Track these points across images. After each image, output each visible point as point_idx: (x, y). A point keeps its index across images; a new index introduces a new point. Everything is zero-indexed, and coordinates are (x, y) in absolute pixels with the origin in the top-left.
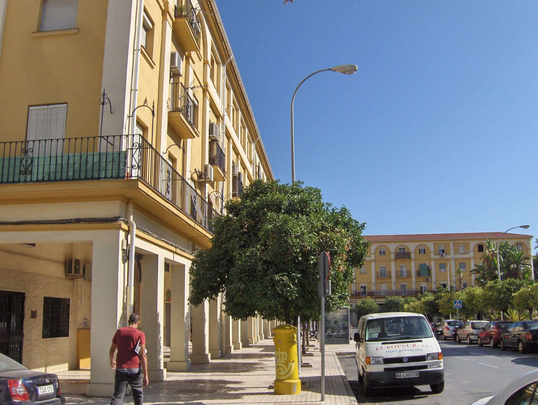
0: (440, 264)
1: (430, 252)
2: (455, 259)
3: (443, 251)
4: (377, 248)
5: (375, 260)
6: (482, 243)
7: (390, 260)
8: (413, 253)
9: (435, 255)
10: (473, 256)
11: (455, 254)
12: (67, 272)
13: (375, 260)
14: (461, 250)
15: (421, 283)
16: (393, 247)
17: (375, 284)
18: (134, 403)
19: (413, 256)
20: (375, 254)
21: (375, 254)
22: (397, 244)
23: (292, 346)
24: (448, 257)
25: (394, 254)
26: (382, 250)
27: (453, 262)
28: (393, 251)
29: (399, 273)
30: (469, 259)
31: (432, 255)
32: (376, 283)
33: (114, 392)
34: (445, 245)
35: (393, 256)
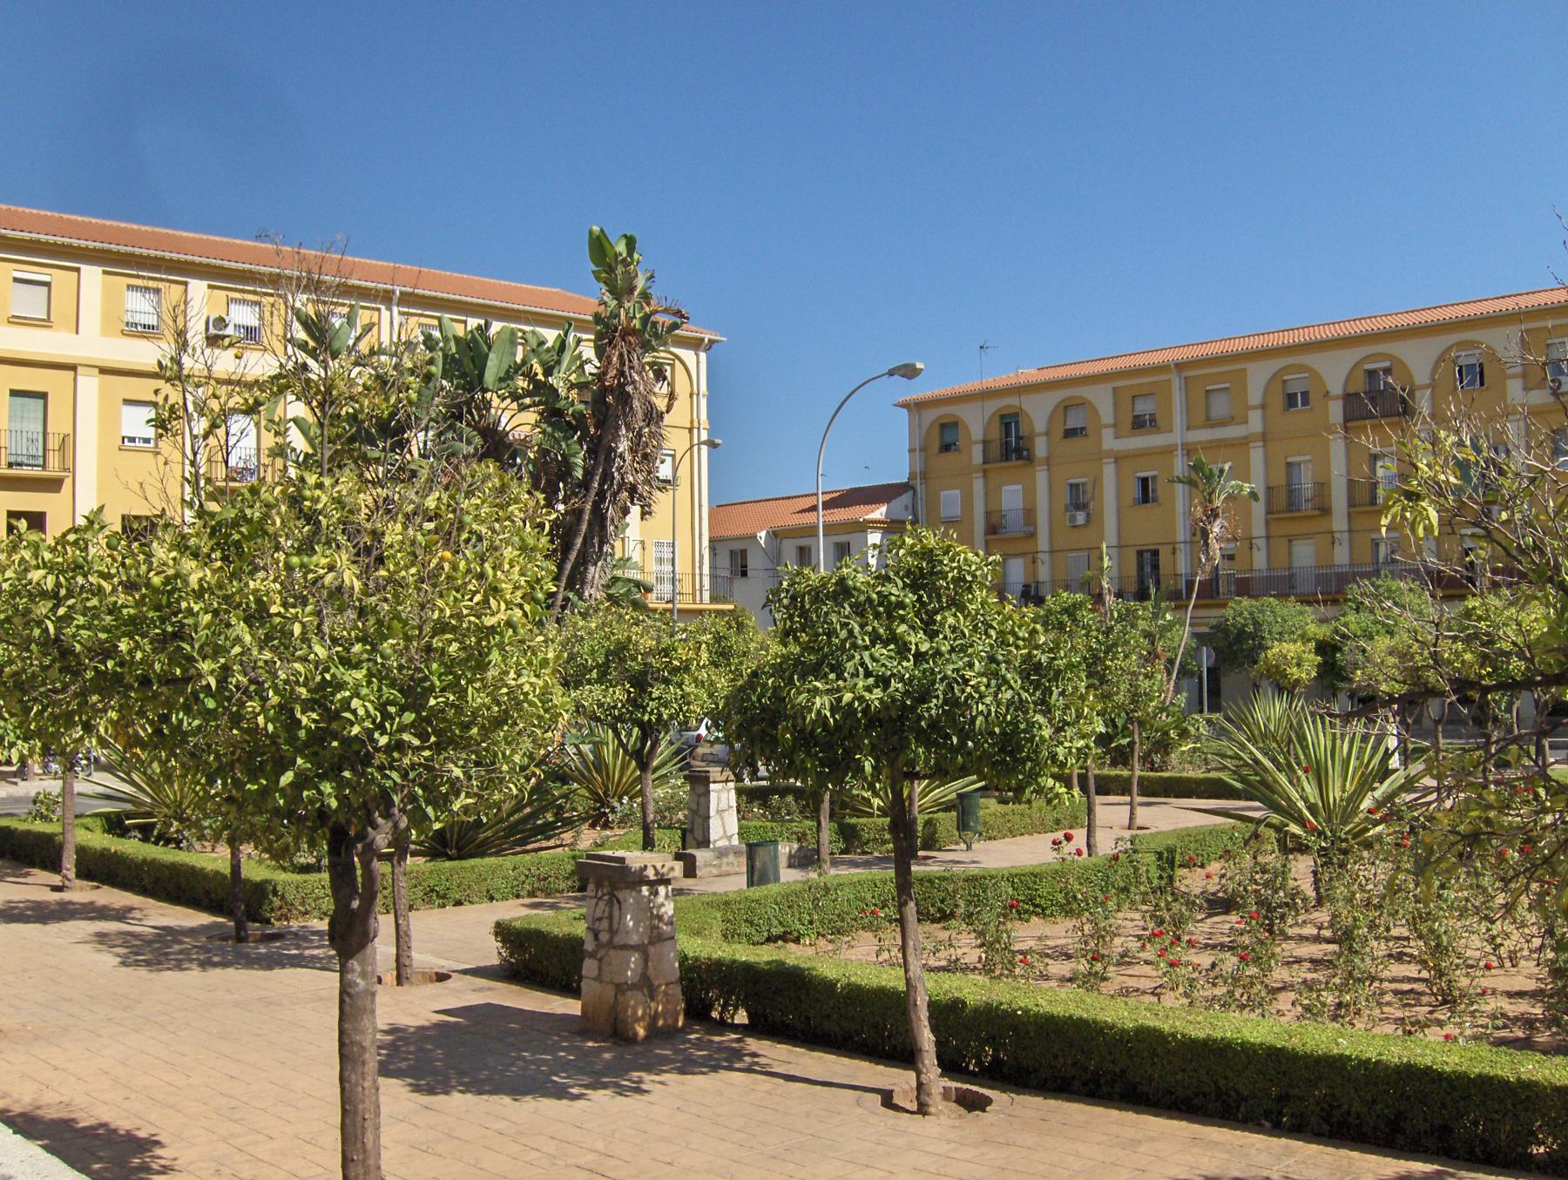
4: (1441, 359)
5: (1264, 437)
7: (1330, 429)
9: (1526, 389)
12: (1299, 514)
14: (1220, 407)
16: (1335, 373)
19: (1040, 448)
20: (1263, 407)
21: (1263, 407)
22: (1350, 357)
23: (768, 973)
25: (1340, 403)
26: (1297, 388)
28: (1336, 388)
29: (1364, 495)
31: (1514, 389)
35: (1336, 411)
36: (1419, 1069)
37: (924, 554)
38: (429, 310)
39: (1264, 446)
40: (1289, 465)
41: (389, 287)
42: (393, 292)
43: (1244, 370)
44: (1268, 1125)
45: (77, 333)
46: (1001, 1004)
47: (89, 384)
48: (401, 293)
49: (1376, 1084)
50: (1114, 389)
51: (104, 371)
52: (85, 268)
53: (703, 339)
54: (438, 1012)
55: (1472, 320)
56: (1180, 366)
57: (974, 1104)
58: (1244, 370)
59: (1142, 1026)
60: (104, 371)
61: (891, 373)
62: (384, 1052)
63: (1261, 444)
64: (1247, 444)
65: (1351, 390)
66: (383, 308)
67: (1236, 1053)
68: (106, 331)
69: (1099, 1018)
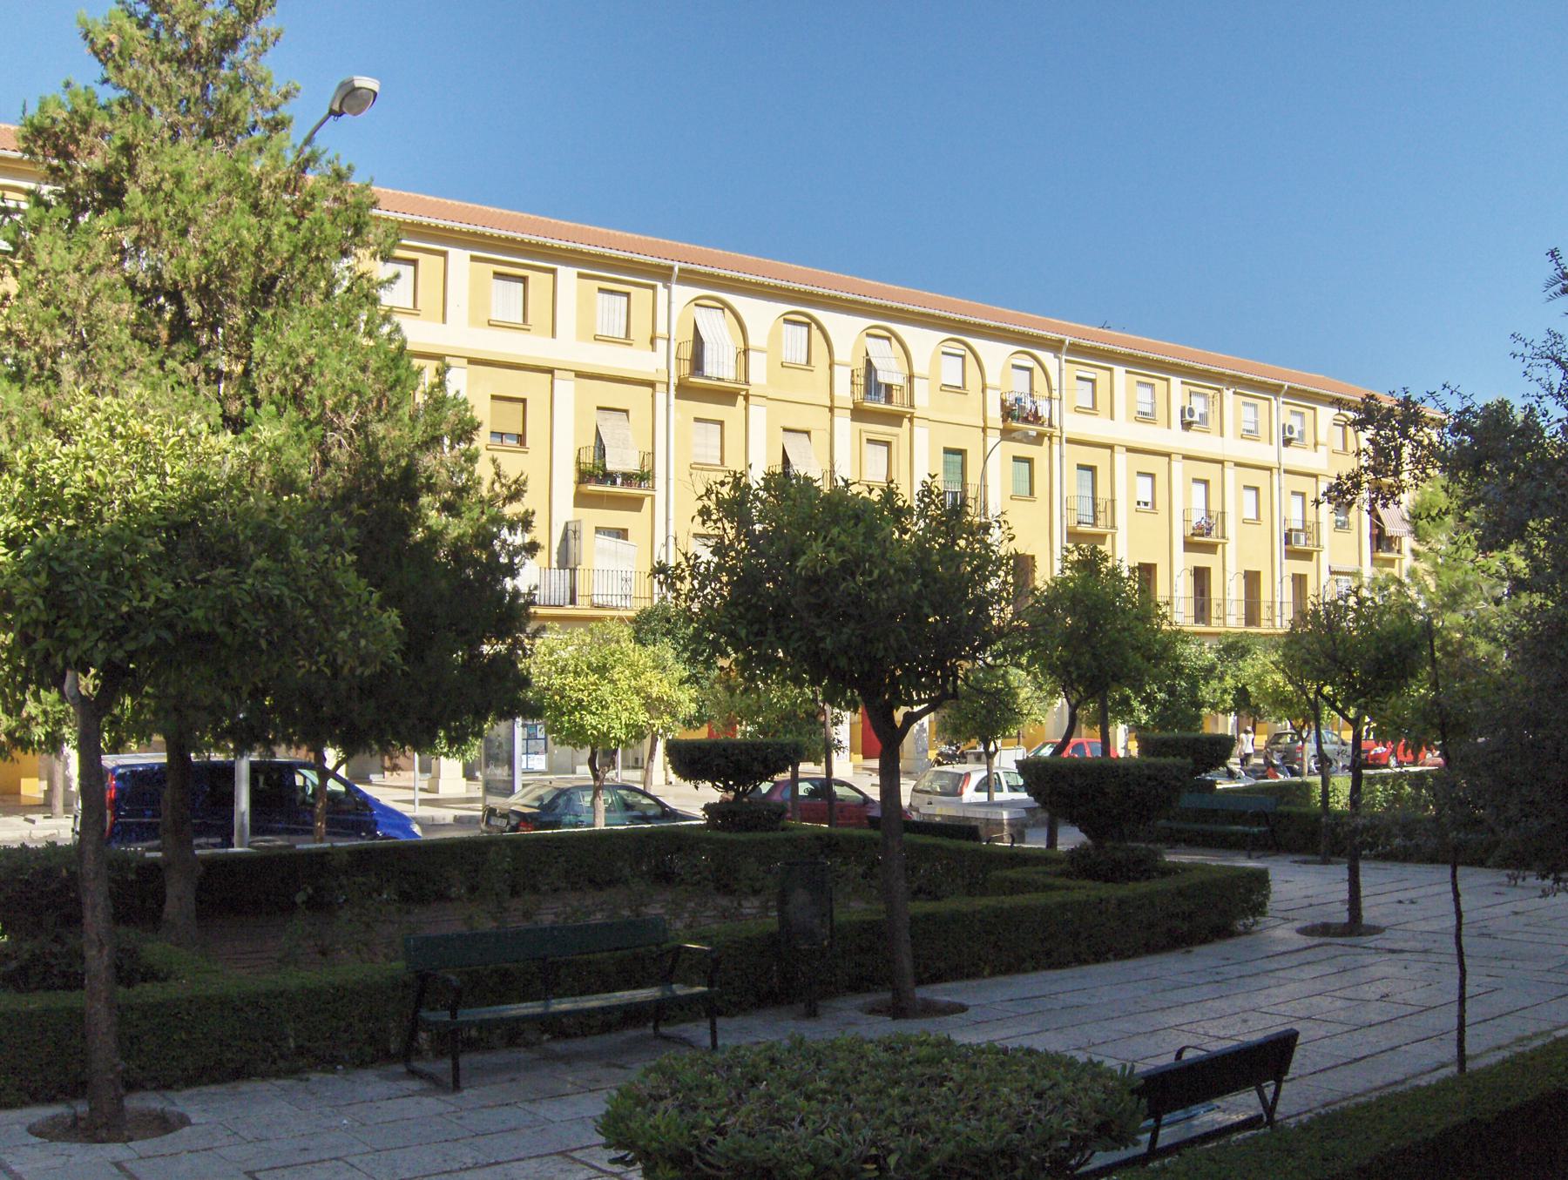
37: (1393, 495)
38: (1087, 358)
41: (669, 263)
42: (671, 268)
45: (554, 335)
47: (566, 388)
48: (681, 270)
51: (580, 375)
52: (561, 270)
53: (1282, 386)
54: (962, 1008)
60: (580, 375)
62: (1342, 783)
66: (660, 285)
68: (473, 321)
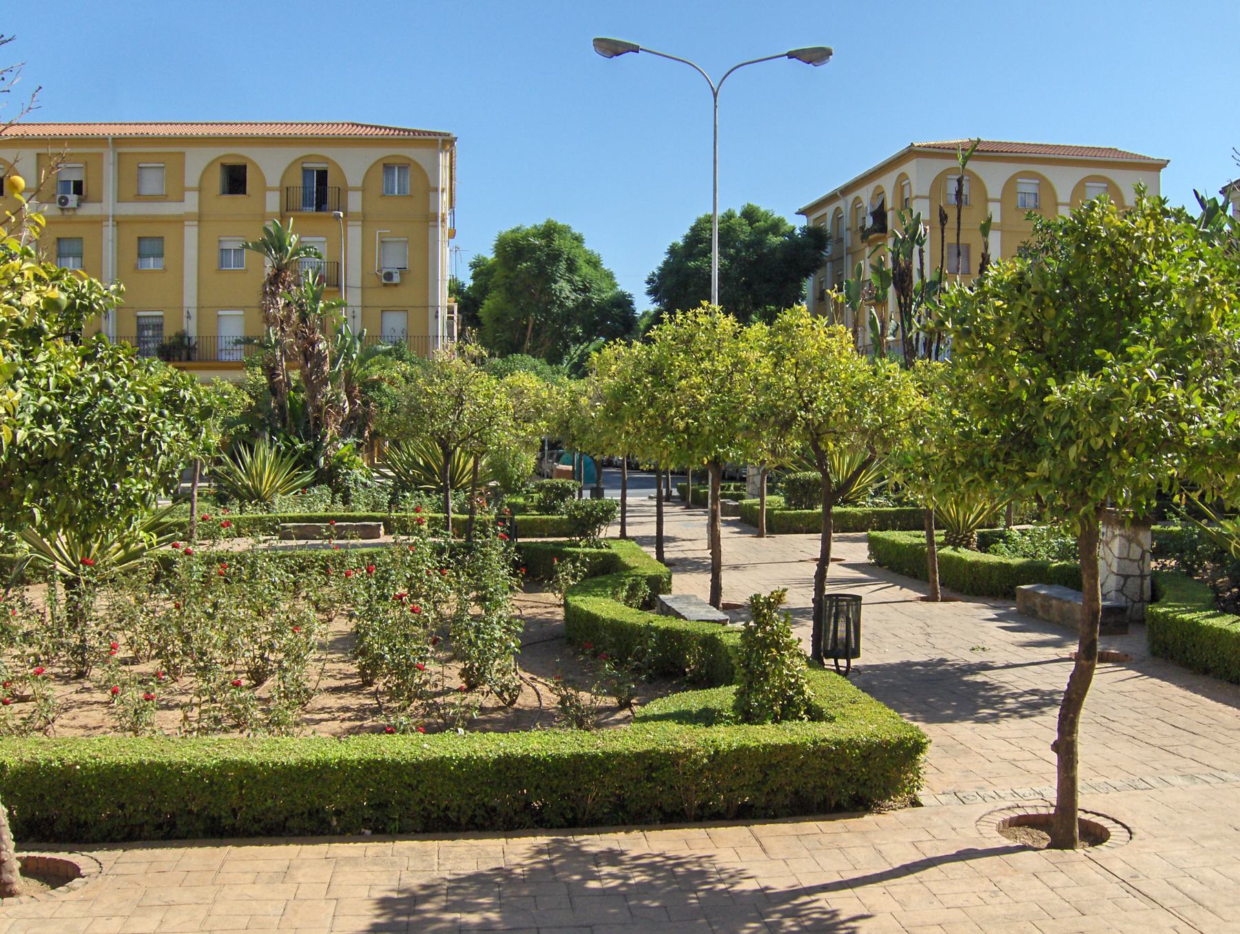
0: (59, 239)
1: (265, 189)
2: (119, 222)
3: (78, 187)
5: (200, 218)
6: (242, 157)
8: (355, 189)
10: (195, 209)
11: (120, 199)
13: (200, 218)
14: (152, 183)
15: (220, 313)
17: (358, 311)
18: (1080, 814)
21: (200, 190)
24: (89, 210)
27: (109, 232)
30: (179, 221)
32: (364, 307)
33: (1056, 737)
34: (86, 163)
36: (516, 759)
39: (199, 226)
40: (220, 241)
43: (184, 154)
44: (368, 832)
46: (51, 762)
49: (476, 778)
50: (38, 155)
55: (319, 139)
56: (118, 141)
57: (58, 876)
58: (184, 154)
59: (225, 761)
61: (791, 55)
63: (196, 223)
64: (183, 222)
65: (288, 184)
67: (333, 771)
69: (174, 759)
